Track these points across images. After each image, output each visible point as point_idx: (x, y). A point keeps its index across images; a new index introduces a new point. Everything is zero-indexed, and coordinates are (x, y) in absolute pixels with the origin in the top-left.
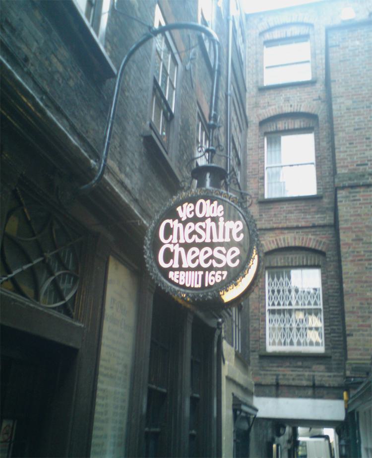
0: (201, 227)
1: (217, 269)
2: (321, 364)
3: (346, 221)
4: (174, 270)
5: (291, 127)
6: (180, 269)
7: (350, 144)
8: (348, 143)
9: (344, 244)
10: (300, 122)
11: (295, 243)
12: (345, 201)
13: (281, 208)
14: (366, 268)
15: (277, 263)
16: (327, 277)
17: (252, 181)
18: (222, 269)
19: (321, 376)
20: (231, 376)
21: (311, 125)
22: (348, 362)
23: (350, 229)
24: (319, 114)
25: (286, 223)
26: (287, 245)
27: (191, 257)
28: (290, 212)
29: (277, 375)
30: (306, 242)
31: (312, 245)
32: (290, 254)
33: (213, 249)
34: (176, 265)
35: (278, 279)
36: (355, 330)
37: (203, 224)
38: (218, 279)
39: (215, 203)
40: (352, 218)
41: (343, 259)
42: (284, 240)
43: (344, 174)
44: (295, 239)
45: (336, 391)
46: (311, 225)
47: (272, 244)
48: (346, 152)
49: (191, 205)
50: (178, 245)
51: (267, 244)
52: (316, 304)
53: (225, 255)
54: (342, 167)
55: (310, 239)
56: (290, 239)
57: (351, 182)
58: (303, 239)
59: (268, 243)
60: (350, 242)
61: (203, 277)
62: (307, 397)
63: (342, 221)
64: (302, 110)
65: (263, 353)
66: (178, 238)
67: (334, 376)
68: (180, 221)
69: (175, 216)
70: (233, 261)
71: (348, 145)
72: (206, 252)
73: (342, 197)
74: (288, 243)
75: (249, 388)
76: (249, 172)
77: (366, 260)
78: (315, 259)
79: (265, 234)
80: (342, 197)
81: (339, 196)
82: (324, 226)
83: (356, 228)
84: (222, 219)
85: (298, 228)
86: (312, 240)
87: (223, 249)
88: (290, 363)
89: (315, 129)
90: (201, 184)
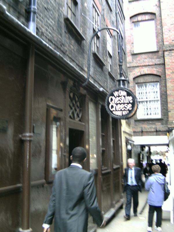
2: (159, 122)
3: (168, 65)
4: (114, 111)
5: (144, 19)
6: (116, 110)
7: (169, 31)
8: (168, 31)
9: (167, 75)
10: (148, 16)
12: (168, 57)
16: (162, 86)
17: (128, 45)
19: (159, 127)
20: (125, 131)
21: (153, 18)
22: (169, 122)
23: (169, 68)
24: (156, 13)
26: (144, 73)
28: (145, 58)
29: (142, 128)
31: (155, 73)
34: (115, 110)
35: (141, 87)
40: (171, 64)
41: (167, 81)
42: (143, 71)
43: (167, 44)
44: (148, 70)
45: (165, 133)
46: (154, 64)
47: (138, 73)
48: (168, 35)
51: (136, 73)
52: (157, 97)
54: (166, 41)
55: (154, 70)
56: (146, 71)
57: (170, 48)
58: (151, 70)
59: (137, 73)
60: (170, 74)
65: (136, 119)
67: (165, 127)
68: (115, 97)
69: (113, 95)
71: (168, 32)
73: (166, 55)
74: (145, 72)
75: (131, 134)
78: (156, 79)
79: (135, 69)
80: (166, 55)
81: (165, 54)
82: (160, 64)
83: (172, 68)
84: (126, 96)
85: (149, 65)
86: (155, 71)
88: (147, 123)
89: (155, 19)
90: (119, 84)
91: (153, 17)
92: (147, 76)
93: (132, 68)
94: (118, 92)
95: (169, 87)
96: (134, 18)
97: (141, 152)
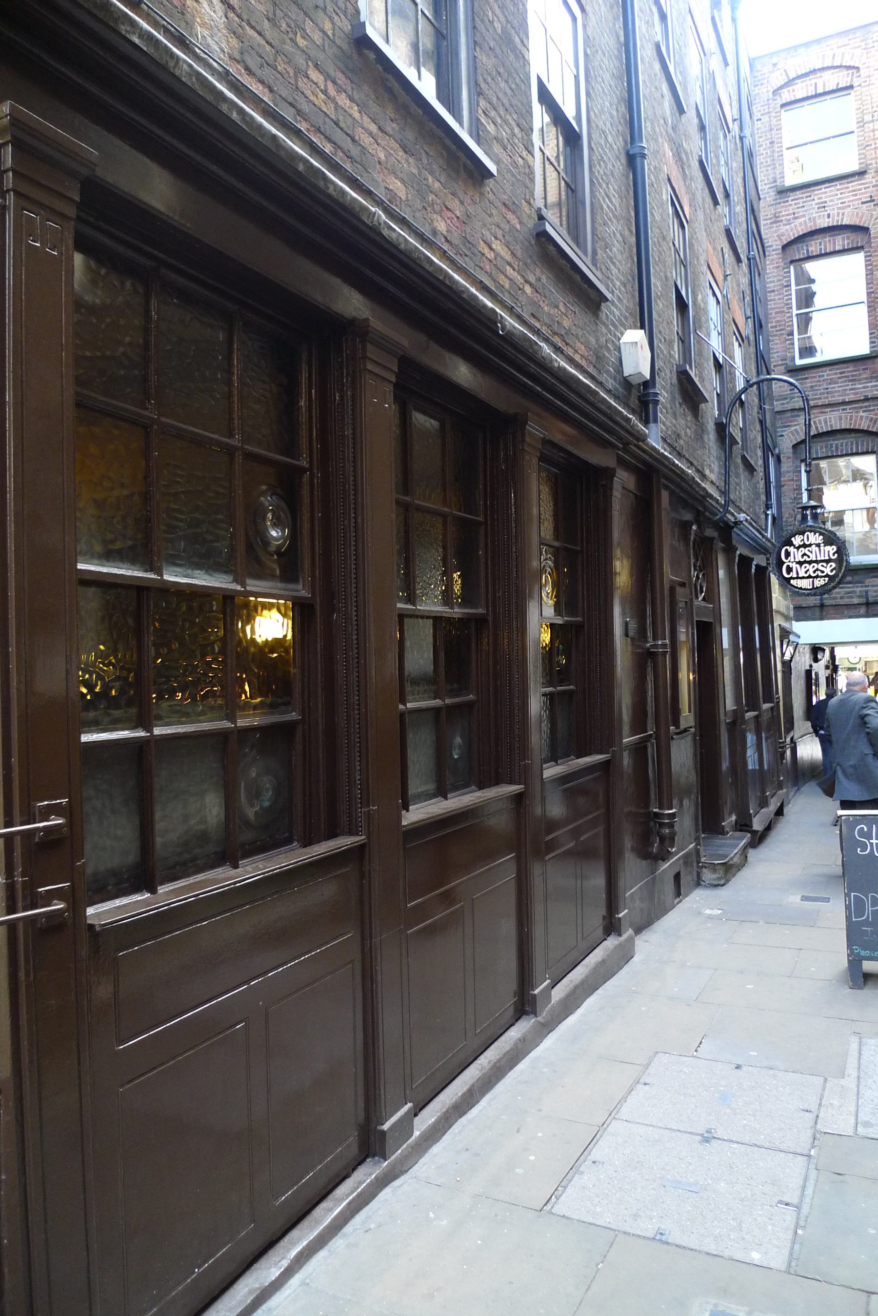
0: (809, 550)
4: (794, 578)
6: (798, 578)
10: (843, 239)
11: (841, 424)
13: (820, 376)
25: (827, 398)
27: (804, 570)
28: (832, 381)
30: (856, 422)
31: (864, 426)
37: (810, 549)
38: (822, 582)
39: (817, 534)
42: (826, 422)
44: (841, 419)
49: (801, 536)
55: (862, 417)
58: (851, 419)
61: (813, 581)
64: (846, 222)
66: (795, 558)
68: (795, 548)
69: (791, 544)
70: (832, 571)
72: (814, 567)
74: (831, 426)
76: (772, 327)
78: (868, 445)
85: (844, 403)
87: (824, 564)
91: (859, 239)
92: (839, 436)
93: (789, 414)
94: (803, 535)
96: (795, 247)
97: (811, 666)
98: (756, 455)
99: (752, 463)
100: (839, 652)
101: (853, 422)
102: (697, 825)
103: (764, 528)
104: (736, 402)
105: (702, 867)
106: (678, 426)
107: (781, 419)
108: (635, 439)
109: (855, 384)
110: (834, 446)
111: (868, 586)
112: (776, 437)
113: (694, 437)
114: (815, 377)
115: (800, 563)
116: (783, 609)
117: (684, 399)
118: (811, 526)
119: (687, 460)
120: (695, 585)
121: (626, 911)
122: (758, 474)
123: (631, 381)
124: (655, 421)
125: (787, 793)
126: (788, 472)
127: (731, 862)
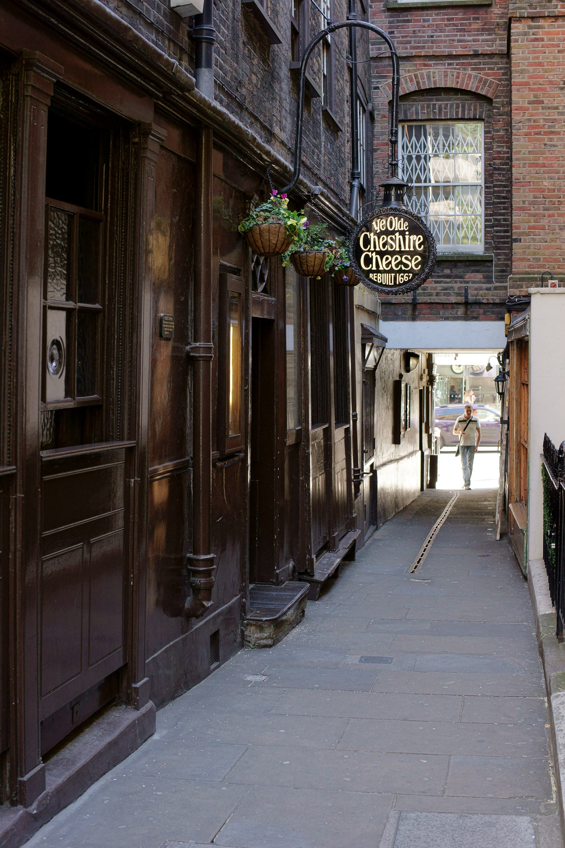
0: (391, 239)
1: (405, 272)
3: (522, 72)
4: (373, 272)
6: (378, 271)
11: (446, 81)
13: (424, 21)
14: (545, 145)
15: (417, 113)
18: (408, 272)
19: (476, 289)
25: (432, 47)
27: (384, 263)
31: (472, 86)
32: (437, 100)
33: (401, 257)
34: (374, 268)
35: (418, 139)
36: (523, 234)
38: (406, 279)
40: (531, 69)
44: (446, 76)
47: (410, 84)
50: (374, 253)
53: (411, 261)
55: (470, 76)
58: (458, 77)
62: (456, 318)
63: (516, 72)
66: (375, 247)
69: (369, 229)
70: (416, 265)
77: (546, 133)
78: (475, 109)
82: (491, 55)
85: (450, 56)
95: (518, 65)
97: (401, 376)
98: (342, 110)
99: (337, 120)
100: (439, 359)
101: (460, 80)
102: (242, 574)
103: (348, 202)
104: (319, 41)
105: (247, 625)
106: (240, 71)
107: (377, 67)
108: (178, 88)
109: (464, 36)
110: (437, 106)
111: (468, 282)
112: (370, 90)
113: (262, 85)
114: (419, 21)
115: (381, 254)
116: (368, 306)
117: (250, 38)
118: (395, 209)
119: (251, 114)
120: (254, 273)
121: (146, 679)
122: (344, 134)
123: (179, 12)
124: (209, 65)
125: (362, 535)
126: (383, 134)
127: (284, 618)
